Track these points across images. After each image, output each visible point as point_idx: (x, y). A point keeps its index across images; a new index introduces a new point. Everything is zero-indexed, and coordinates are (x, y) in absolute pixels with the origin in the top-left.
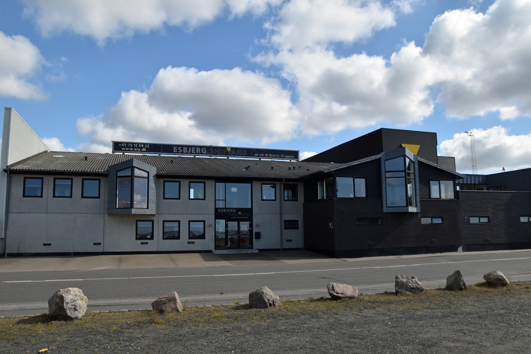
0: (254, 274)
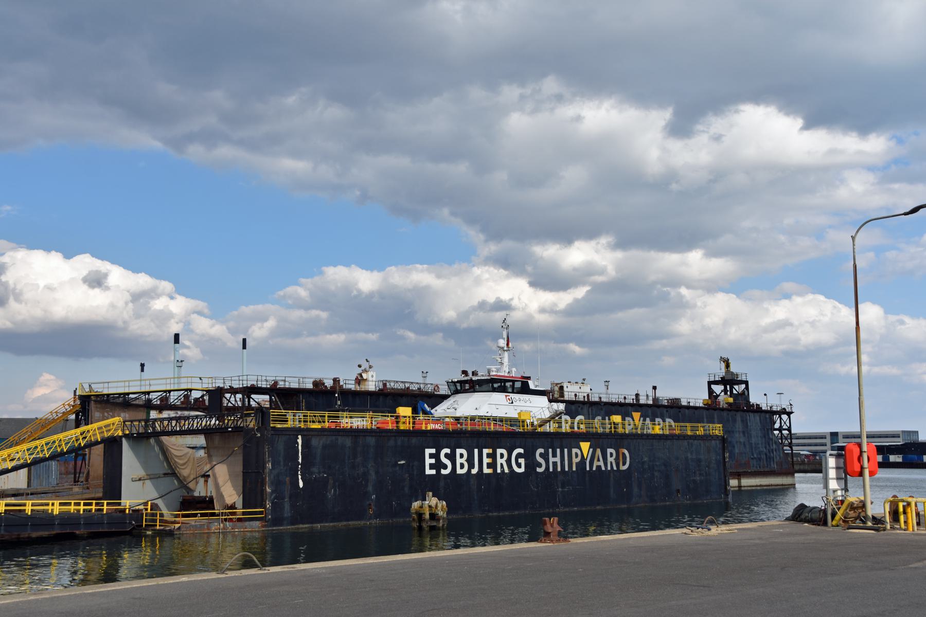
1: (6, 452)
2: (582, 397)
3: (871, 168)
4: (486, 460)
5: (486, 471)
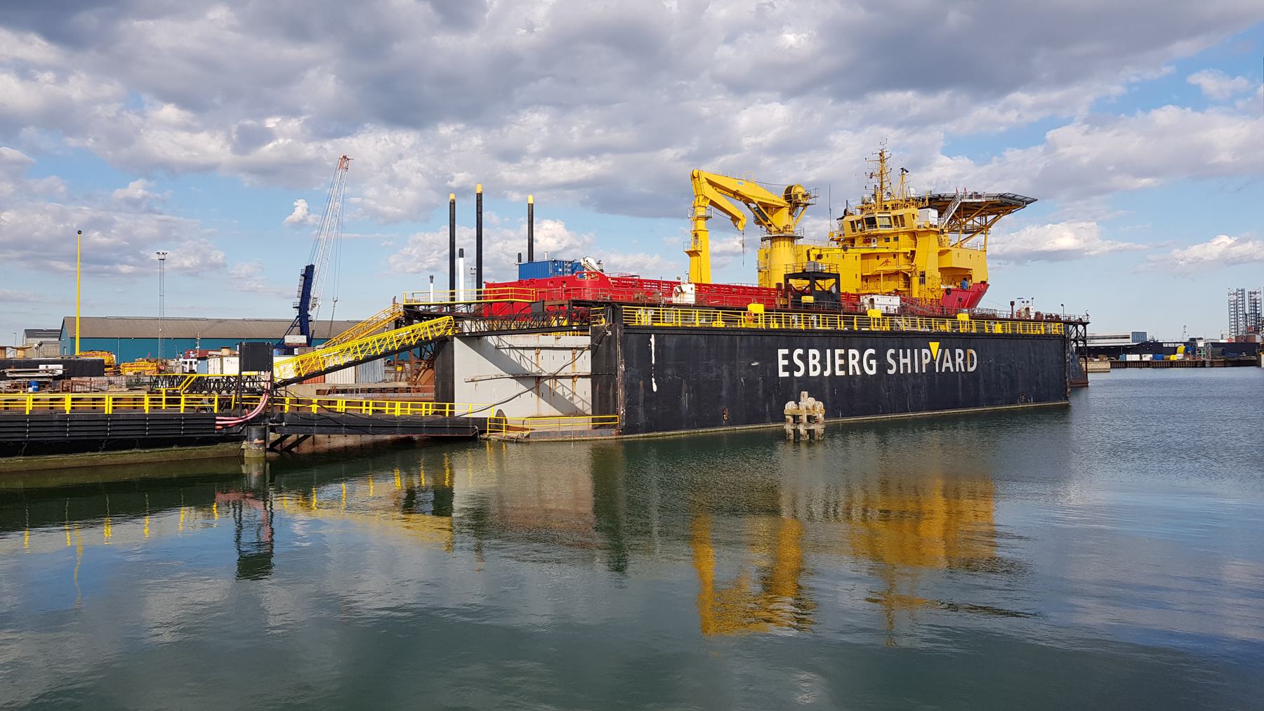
5: (839, 373)
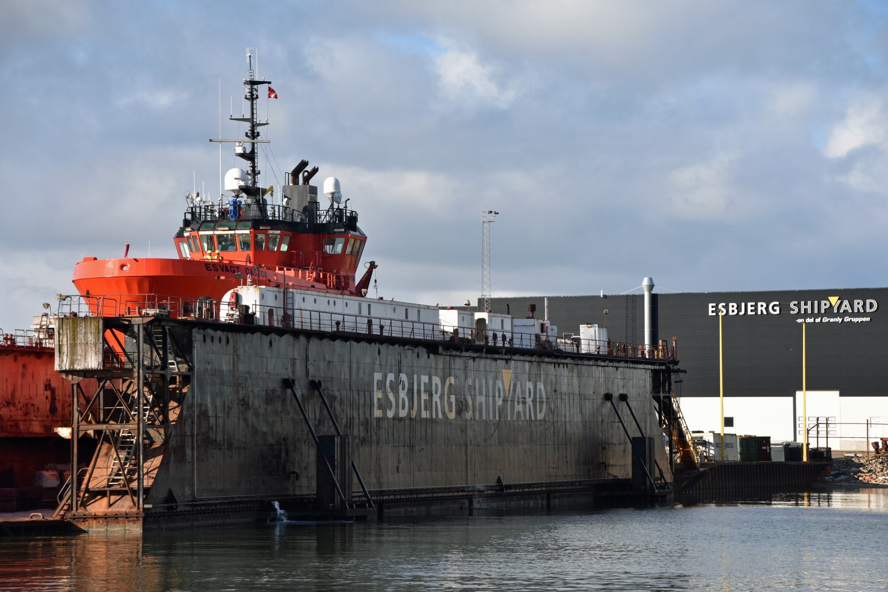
0: (112, 413)
1: (849, 308)
2: (378, 327)
3: (308, 342)
4: (749, 308)
